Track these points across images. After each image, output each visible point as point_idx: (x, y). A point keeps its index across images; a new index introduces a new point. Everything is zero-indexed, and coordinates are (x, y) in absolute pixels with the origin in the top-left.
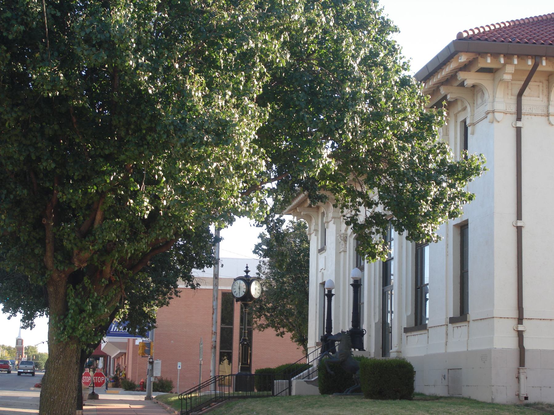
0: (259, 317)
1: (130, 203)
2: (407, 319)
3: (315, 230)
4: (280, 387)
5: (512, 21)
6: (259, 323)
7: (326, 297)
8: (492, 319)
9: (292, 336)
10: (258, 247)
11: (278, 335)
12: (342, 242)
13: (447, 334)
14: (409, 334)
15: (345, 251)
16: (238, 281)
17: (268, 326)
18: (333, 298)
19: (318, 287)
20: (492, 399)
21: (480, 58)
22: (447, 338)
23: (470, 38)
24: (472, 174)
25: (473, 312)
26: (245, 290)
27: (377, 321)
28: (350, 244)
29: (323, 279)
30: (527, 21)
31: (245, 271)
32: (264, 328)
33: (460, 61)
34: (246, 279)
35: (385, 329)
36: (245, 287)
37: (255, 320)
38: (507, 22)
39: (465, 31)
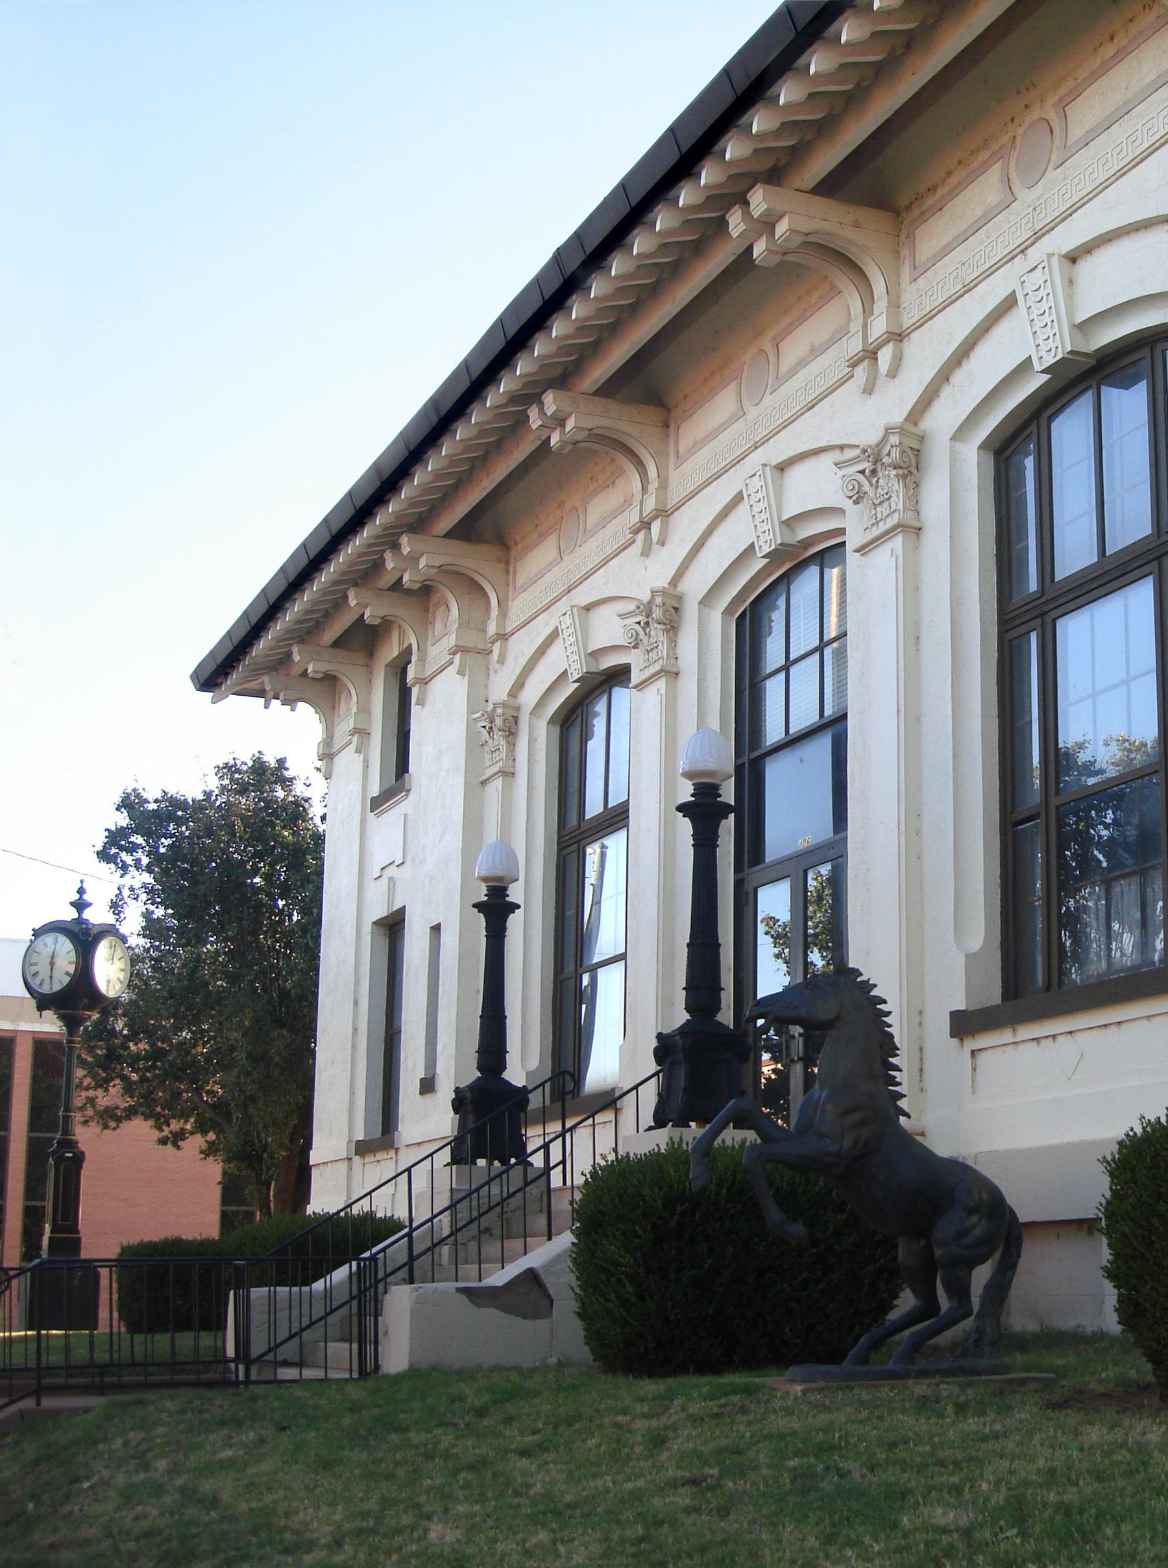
3: (356, 731)
4: (305, 1306)
9: (204, 1146)
10: (116, 839)
11: (163, 1141)
12: (499, 738)
15: (508, 774)
16: (49, 939)
17: (131, 1113)
18: (515, 922)
26: (72, 969)
28: (532, 741)
31: (72, 904)
32: (119, 1120)
34: (76, 929)
36: (73, 956)
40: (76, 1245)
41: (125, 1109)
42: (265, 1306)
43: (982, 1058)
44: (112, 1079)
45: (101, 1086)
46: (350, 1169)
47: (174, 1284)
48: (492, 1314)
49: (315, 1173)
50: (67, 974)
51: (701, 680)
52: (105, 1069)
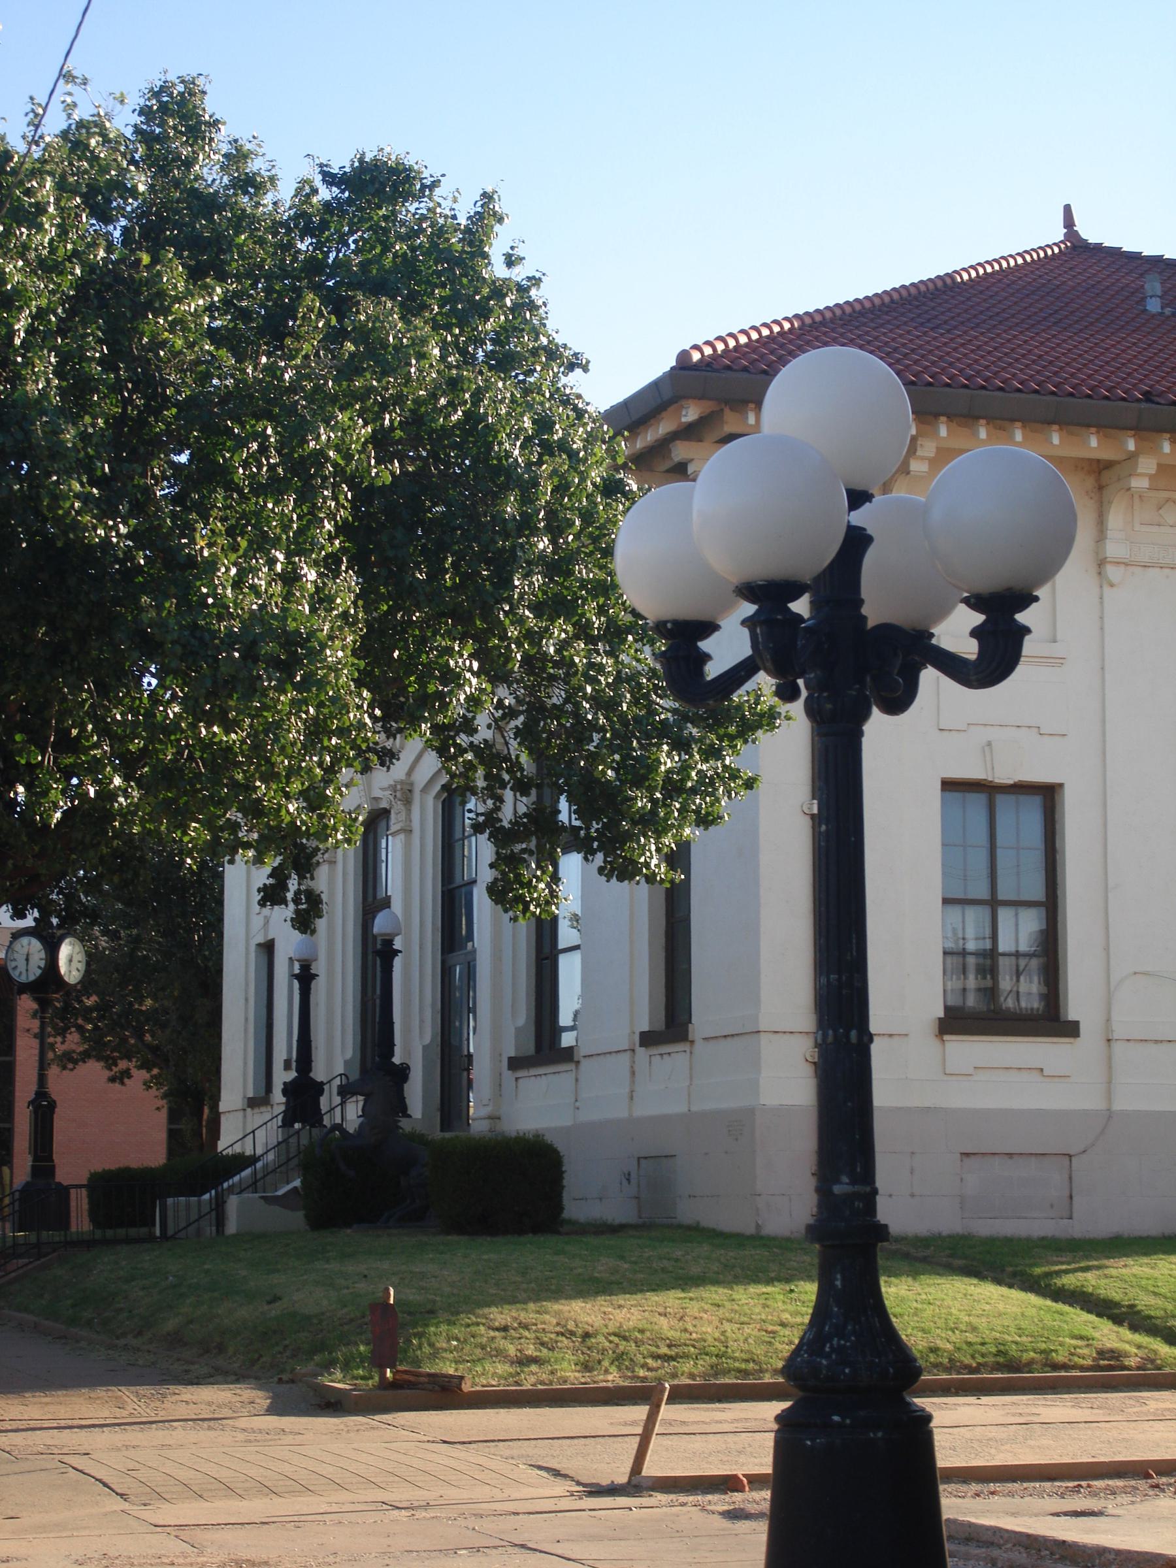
0: (63, 1032)
1: (16, 794)
2: (517, 1037)
5: (796, 316)
6: (60, 1048)
7: (296, 984)
8: (756, 1035)
11: (112, 1080)
13: (633, 1073)
14: (520, 1074)
17: (85, 1056)
19: (253, 955)
20: (758, 1226)
21: (727, 411)
22: (633, 1082)
23: (707, 365)
24: (760, 726)
25: (702, 1020)
26: (42, 963)
27: (427, 1039)
29: (266, 934)
30: (828, 315)
32: (76, 1062)
33: (684, 420)
35: (452, 1063)
36: (43, 955)
37: (51, 1040)
38: (786, 319)
39: (696, 347)
40: (51, 1171)
41: (80, 1054)
42: (179, 1207)
43: (520, 1081)
44: (69, 1028)
45: (59, 1034)
46: (245, 1117)
47: (126, 1199)
48: (277, 1209)
49: (223, 1119)
50: (39, 967)
51: (422, 838)
52: (63, 1019)
